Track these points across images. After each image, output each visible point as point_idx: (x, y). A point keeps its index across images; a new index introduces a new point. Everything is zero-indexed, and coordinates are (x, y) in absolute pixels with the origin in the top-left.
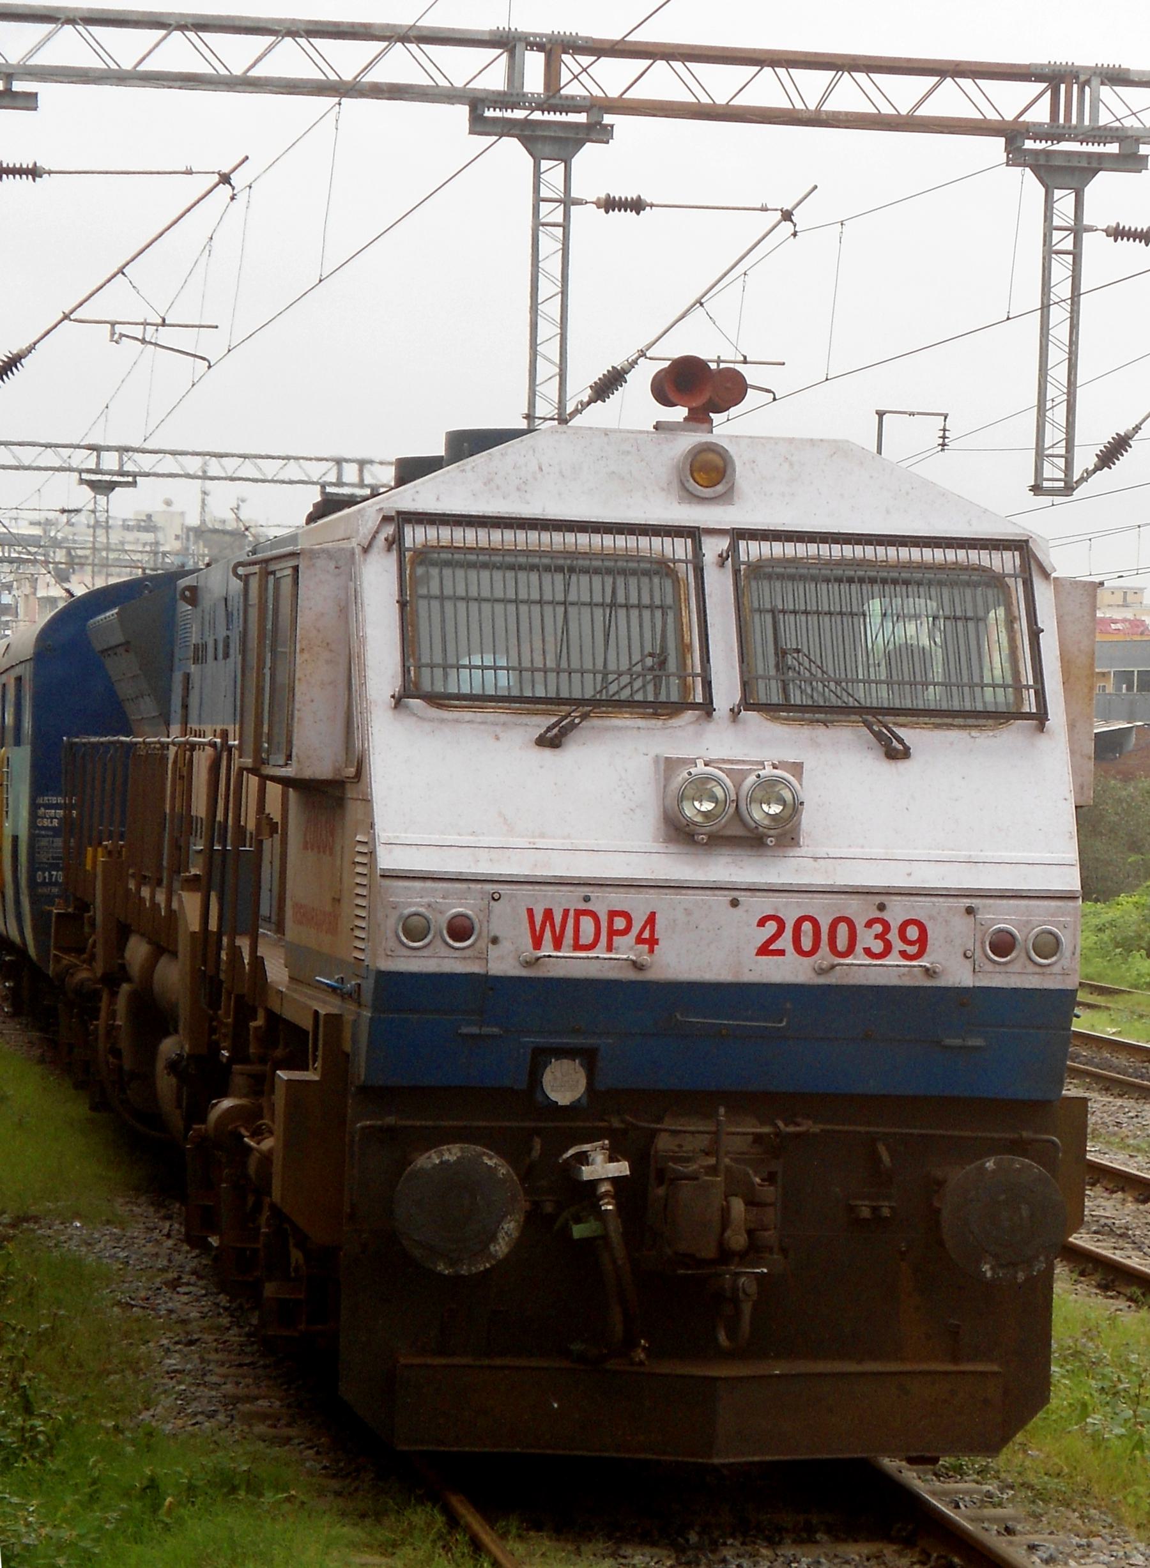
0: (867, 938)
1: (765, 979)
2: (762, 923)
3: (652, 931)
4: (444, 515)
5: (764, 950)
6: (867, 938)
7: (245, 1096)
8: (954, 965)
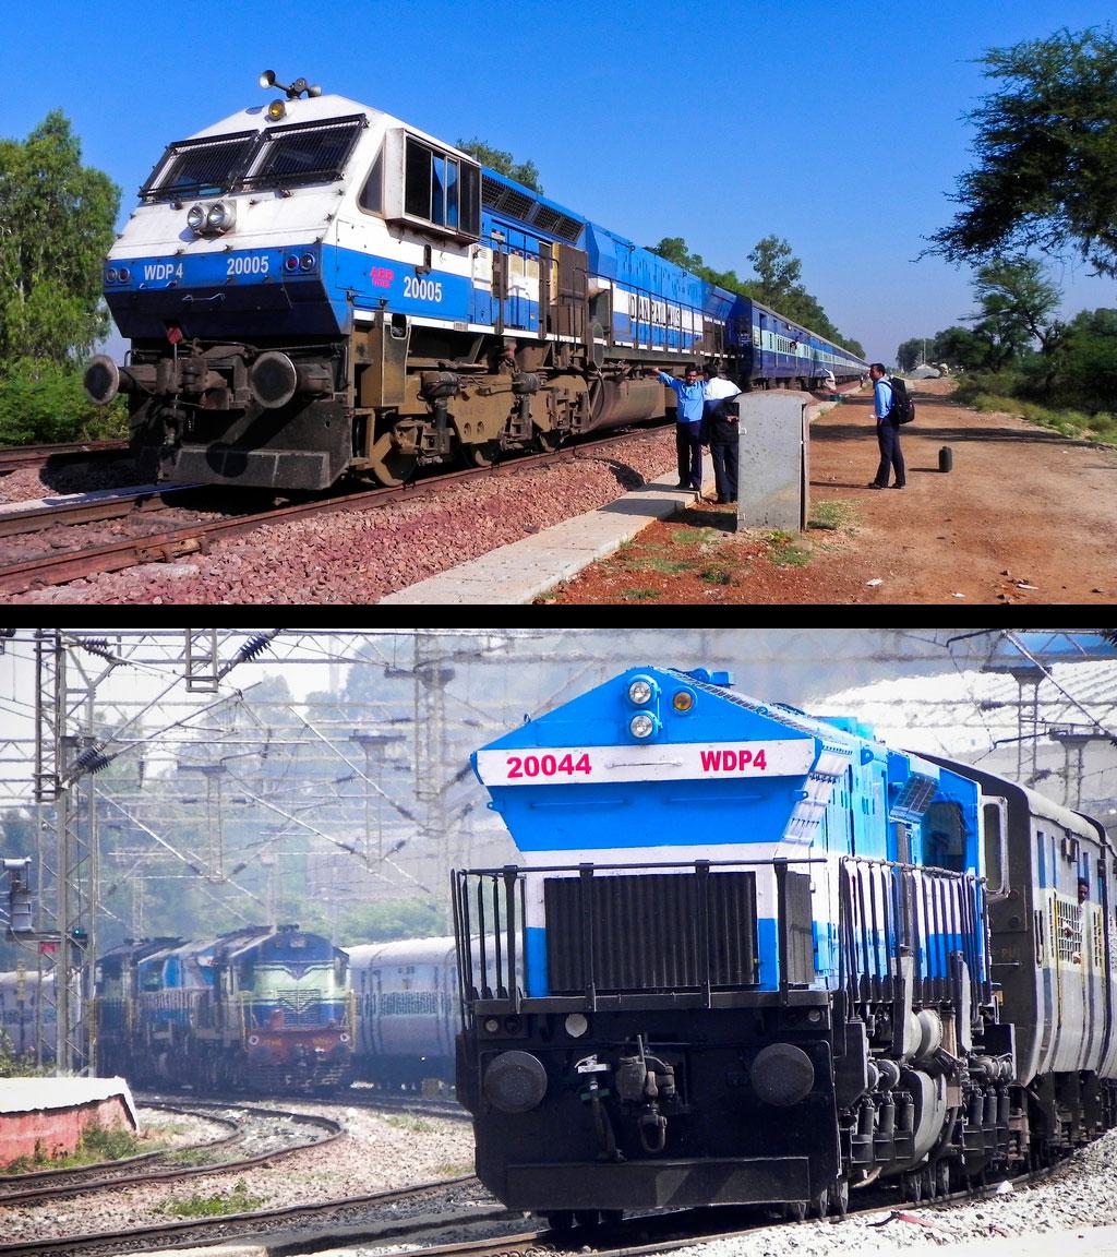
2: (510, 762)
3: (587, 763)
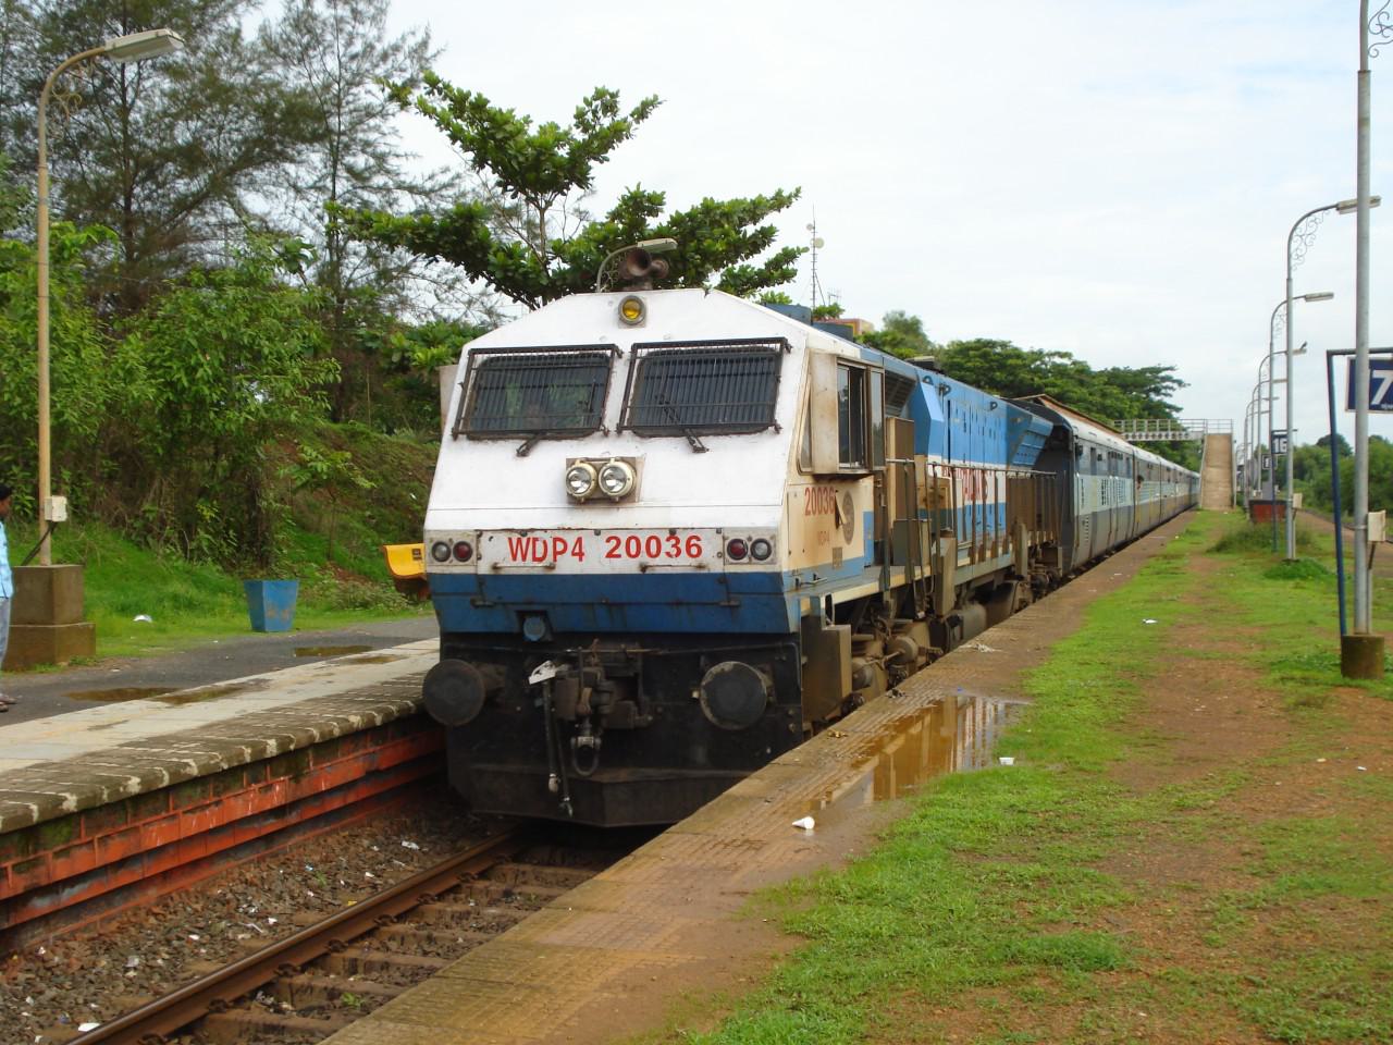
0: (667, 546)
2: (608, 540)
5: (610, 555)
6: (667, 546)
7: (79, 824)
8: (714, 561)
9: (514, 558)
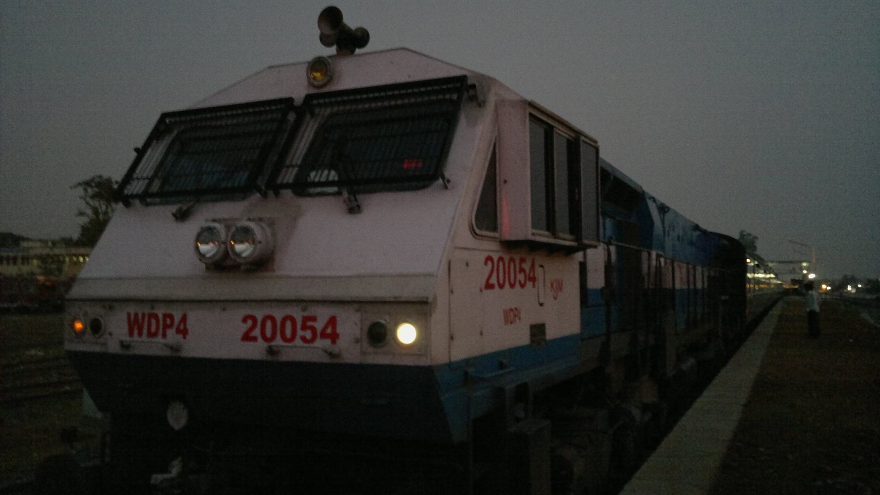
1: (207, 355)
2: (245, 320)
4: (450, 144)
5: (247, 337)
9: (131, 334)
